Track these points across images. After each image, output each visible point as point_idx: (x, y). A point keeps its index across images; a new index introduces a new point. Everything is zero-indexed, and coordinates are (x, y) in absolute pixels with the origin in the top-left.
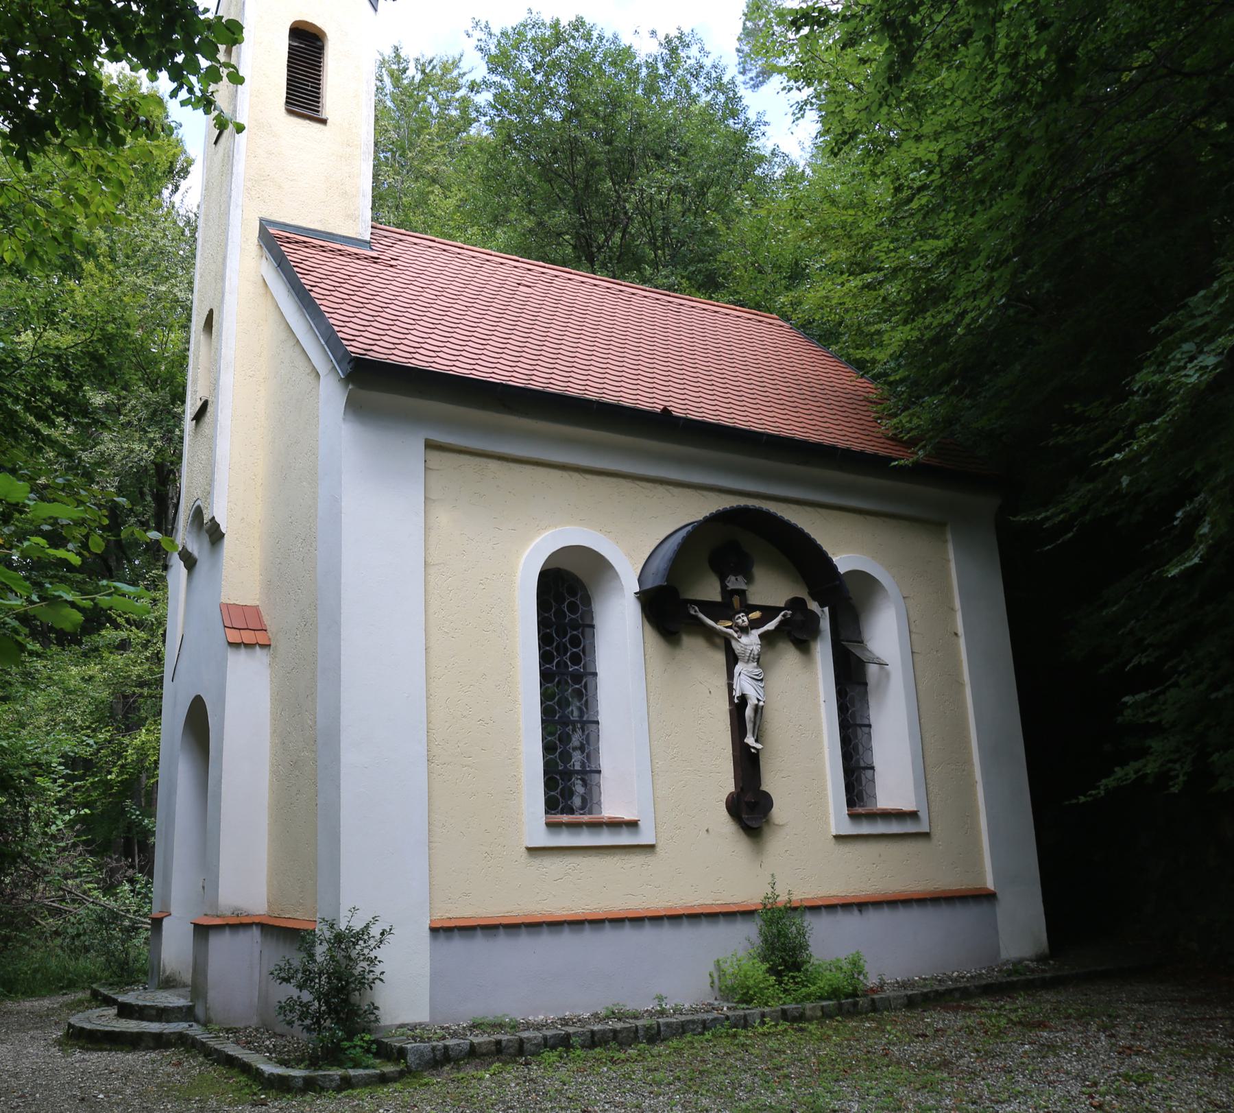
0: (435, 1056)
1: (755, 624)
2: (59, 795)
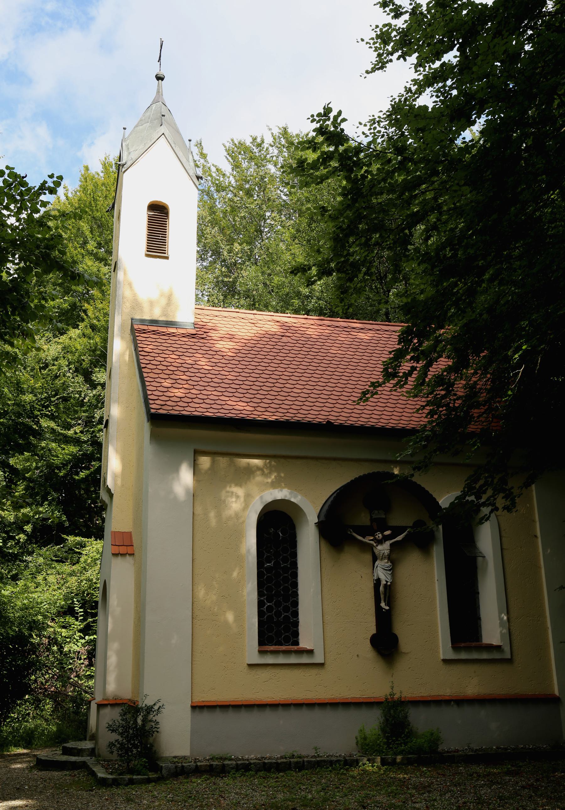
1: (386, 538)
2: (79, 627)
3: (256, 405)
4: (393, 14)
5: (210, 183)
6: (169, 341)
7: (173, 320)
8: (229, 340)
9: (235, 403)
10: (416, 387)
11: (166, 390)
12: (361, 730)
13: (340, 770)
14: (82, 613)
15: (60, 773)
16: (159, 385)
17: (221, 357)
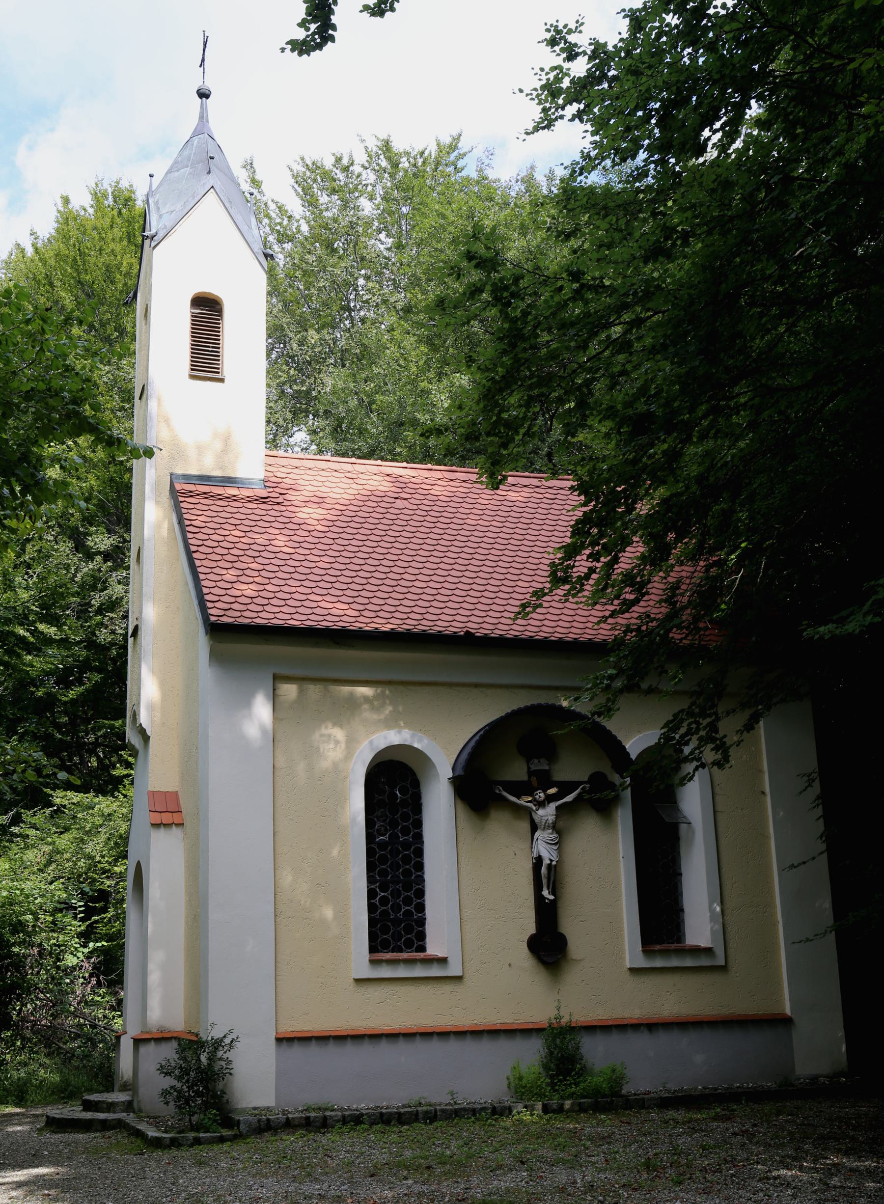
0: (260, 1125)
1: (550, 799)
2: (79, 930)
3: (361, 607)
4: (564, 55)
5: (268, 228)
6: (228, 509)
7: (233, 476)
8: (317, 506)
9: (330, 605)
10: (595, 593)
11: (229, 586)
12: (514, 1068)
13: (486, 1121)
14: (83, 909)
15: (86, 1136)
16: (218, 578)
17: (307, 534)
